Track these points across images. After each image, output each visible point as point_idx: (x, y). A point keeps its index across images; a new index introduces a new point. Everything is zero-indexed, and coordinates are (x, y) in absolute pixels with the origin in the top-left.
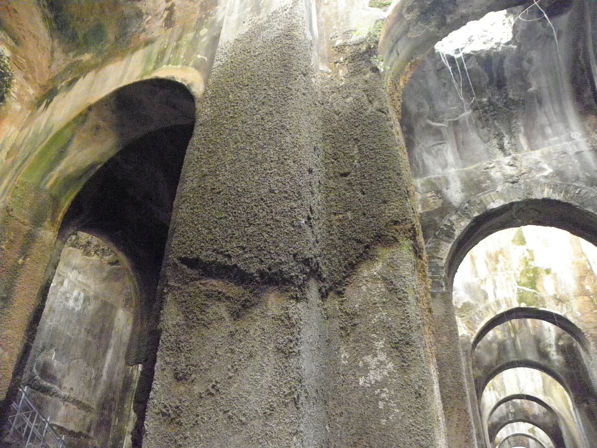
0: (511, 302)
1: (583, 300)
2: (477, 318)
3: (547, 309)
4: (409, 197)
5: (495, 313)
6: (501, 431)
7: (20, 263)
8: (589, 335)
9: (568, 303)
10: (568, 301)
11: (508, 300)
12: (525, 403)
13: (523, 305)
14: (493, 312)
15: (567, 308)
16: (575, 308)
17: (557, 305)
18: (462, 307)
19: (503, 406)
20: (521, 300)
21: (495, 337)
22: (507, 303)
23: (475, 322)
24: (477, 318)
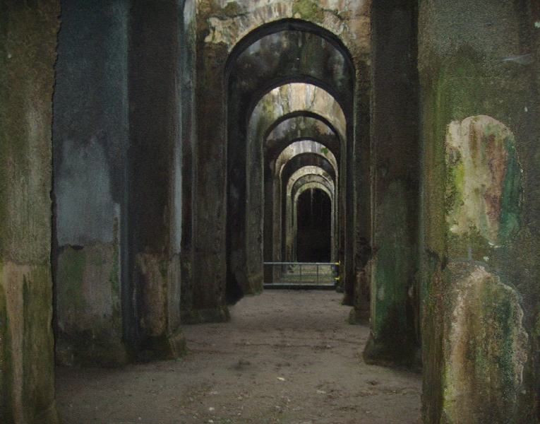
0: (285, 10)
1: (364, 21)
2: (241, 24)
3: (326, 27)
4: (24, 131)
5: (264, 21)
6: (290, 147)
7: (381, 299)
8: (357, 62)
9: (347, 22)
10: (348, 19)
11: (282, 6)
12: (319, 123)
13: (297, 16)
14: (262, 18)
15: (345, 28)
16: (353, 29)
17: (335, 22)
18: (226, 7)
19: (286, 122)
20: (296, 10)
21: (280, 44)
22: (280, 10)
23: (237, 29)
24: (241, 24)
